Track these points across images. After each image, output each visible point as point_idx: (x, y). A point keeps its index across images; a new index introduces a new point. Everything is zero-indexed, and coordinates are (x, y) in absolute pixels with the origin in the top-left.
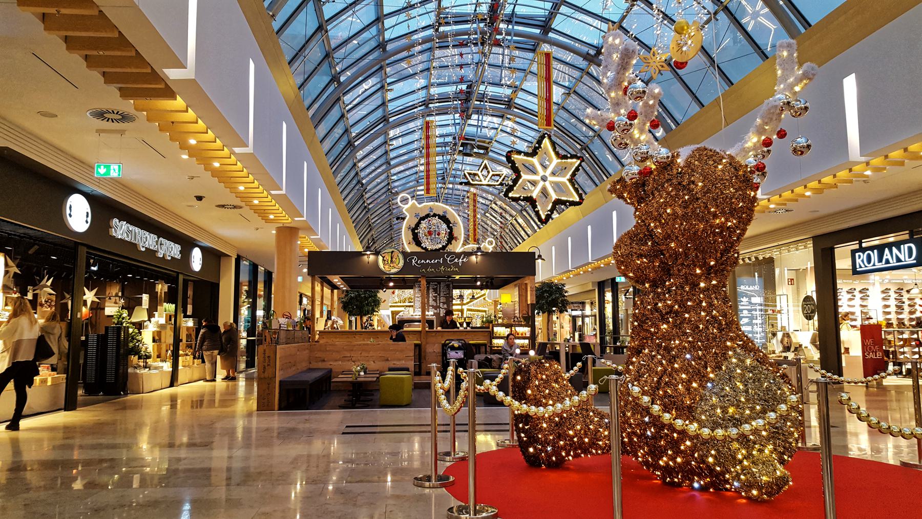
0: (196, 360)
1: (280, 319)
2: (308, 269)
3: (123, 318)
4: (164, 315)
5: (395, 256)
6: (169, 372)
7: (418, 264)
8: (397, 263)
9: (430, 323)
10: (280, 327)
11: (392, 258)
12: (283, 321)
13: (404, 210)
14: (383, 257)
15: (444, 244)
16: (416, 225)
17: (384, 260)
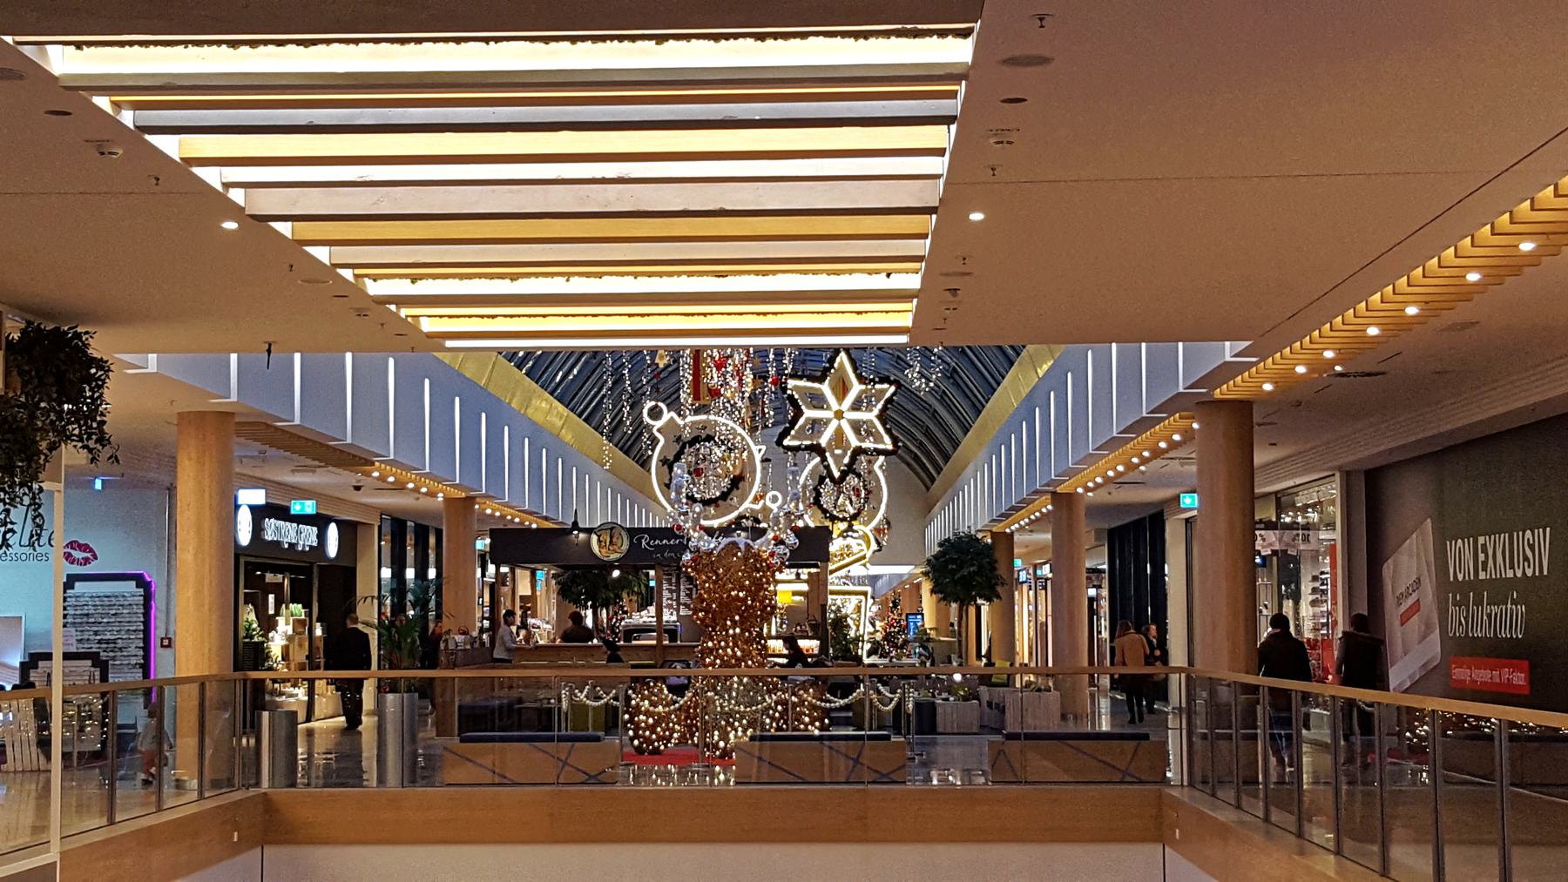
0: (329, 687)
1: (456, 637)
2: (491, 538)
3: (254, 630)
4: (291, 621)
5: (616, 535)
6: (305, 701)
7: (651, 547)
8: (619, 545)
9: (673, 634)
10: (457, 646)
11: (611, 538)
12: (460, 638)
13: (655, 431)
14: (599, 536)
15: (725, 490)
16: (675, 456)
17: (599, 541)
